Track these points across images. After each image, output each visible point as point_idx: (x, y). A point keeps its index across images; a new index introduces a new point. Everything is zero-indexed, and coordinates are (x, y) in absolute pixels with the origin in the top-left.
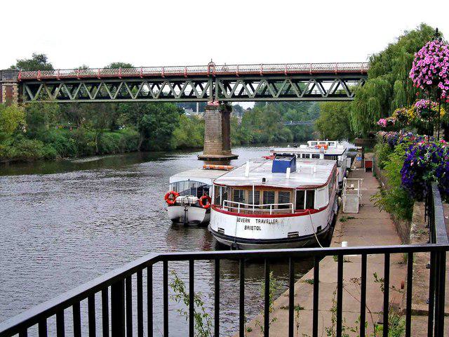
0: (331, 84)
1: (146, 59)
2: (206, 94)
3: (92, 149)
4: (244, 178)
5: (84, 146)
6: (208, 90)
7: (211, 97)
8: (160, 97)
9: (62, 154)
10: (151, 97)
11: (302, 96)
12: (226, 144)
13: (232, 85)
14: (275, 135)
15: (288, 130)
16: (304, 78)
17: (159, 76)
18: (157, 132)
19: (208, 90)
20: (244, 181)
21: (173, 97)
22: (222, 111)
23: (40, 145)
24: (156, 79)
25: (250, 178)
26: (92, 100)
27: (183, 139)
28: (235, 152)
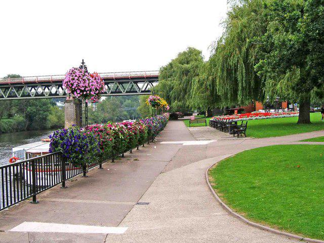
1: (29, 73)
2: (65, 92)
8: (36, 96)
16: (139, 80)
17: (48, 82)
18: (37, 117)
21: (58, 95)
24: (33, 84)
26: (19, 98)
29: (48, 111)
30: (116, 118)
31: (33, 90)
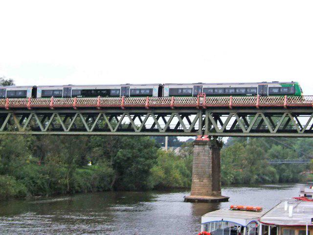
0: (309, 118)
3: (63, 187)
4: (288, 219)
5: (56, 183)
6: (197, 123)
7: (200, 132)
9: (32, 193)
10: (133, 130)
11: (115, 130)
12: (218, 183)
13: (224, 119)
14: (258, 175)
15: (272, 169)
18: (133, 168)
19: (197, 123)
20: (290, 221)
22: (212, 147)
23: (13, 181)
25: (294, 219)
26: (67, 132)
27: (160, 177)
28: (224, 193)
29: (152, 158)
30: (256, 177)
31: (137, 122)
